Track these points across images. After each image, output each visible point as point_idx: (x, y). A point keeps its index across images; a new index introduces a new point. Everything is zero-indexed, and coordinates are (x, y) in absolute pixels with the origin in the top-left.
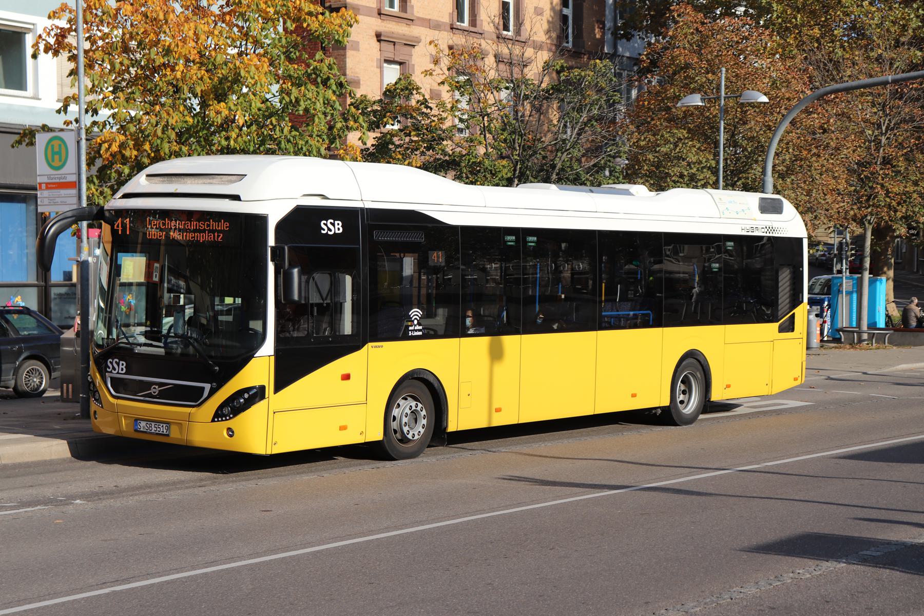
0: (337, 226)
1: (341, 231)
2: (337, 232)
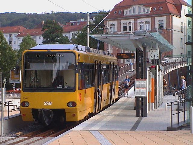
0: (50, 103)
1: (51, 104)
2: (50, 104)
